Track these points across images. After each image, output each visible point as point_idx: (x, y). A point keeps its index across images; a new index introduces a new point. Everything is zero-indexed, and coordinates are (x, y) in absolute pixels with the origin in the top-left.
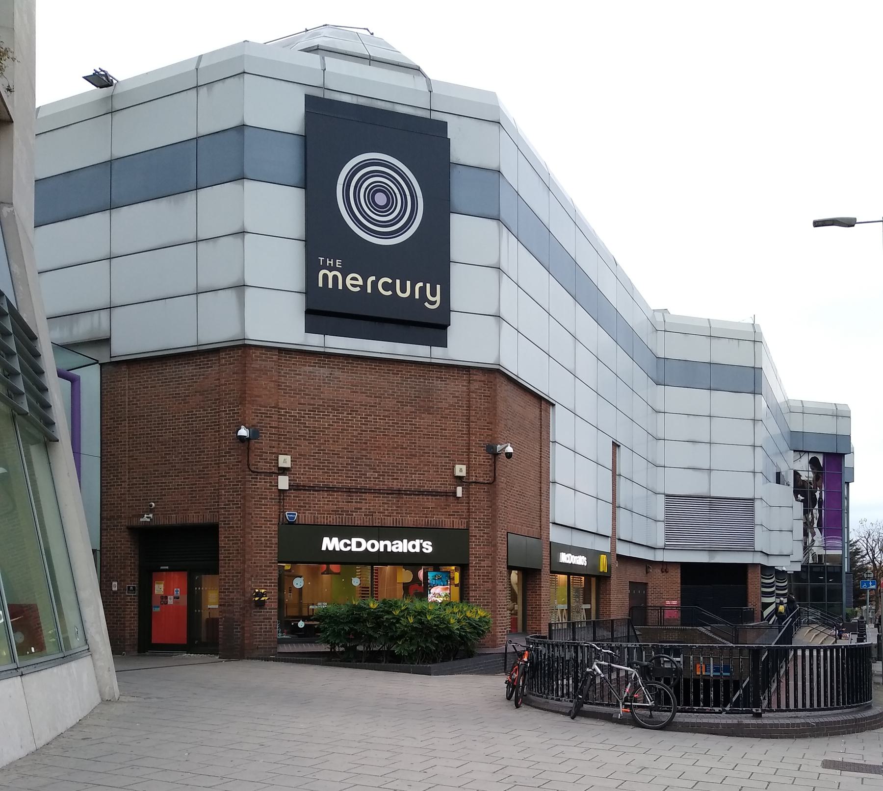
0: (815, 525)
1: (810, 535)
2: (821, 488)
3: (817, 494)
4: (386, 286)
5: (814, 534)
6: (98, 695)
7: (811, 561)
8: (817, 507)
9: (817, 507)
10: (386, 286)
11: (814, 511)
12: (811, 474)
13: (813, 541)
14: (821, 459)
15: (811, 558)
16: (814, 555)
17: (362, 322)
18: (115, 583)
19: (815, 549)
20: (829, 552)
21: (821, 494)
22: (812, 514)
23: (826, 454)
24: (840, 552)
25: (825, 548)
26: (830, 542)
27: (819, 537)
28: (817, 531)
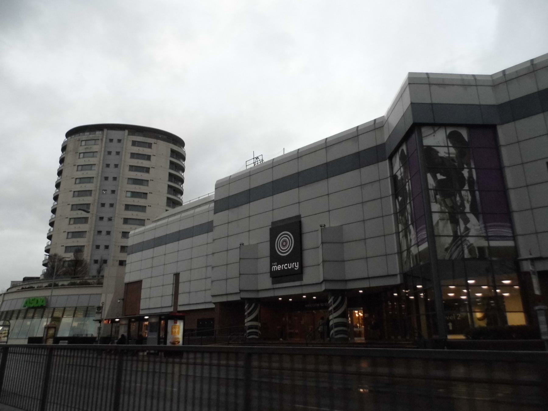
0: (467, 209)
1: (461, 222)
2: (469, 165)
3: (466, 173)
4: (286, 266)
5: (467, 221)
6: (96, 322)
7: (467, 255)
8: (466, 187)
9: (466, 187)
10: (286, 266)
11: (463, 193)
12: (452, 150)
13: (467, 229)
14: (464, 133)
15: (466, 251)
16: (471, 249)
17: (311, 283)
18: (418, 286)
19: (471, 240)
20: (493, 244)
21: (470, 173)
22: (461, 197)
23: (470, 127)
24: (511, 243)
25: (487, 238)
26: (492, 231)
27: (474, 225)
28: (471, 217)
